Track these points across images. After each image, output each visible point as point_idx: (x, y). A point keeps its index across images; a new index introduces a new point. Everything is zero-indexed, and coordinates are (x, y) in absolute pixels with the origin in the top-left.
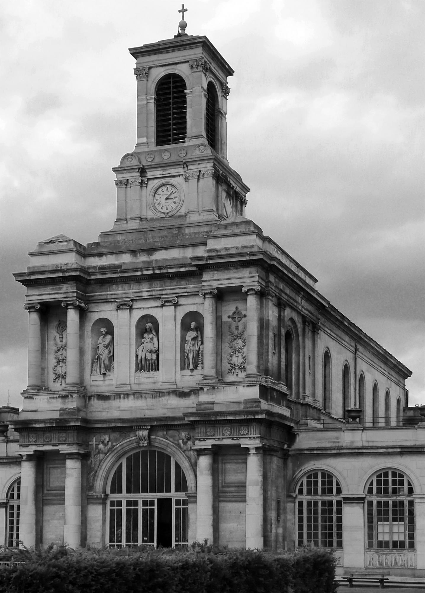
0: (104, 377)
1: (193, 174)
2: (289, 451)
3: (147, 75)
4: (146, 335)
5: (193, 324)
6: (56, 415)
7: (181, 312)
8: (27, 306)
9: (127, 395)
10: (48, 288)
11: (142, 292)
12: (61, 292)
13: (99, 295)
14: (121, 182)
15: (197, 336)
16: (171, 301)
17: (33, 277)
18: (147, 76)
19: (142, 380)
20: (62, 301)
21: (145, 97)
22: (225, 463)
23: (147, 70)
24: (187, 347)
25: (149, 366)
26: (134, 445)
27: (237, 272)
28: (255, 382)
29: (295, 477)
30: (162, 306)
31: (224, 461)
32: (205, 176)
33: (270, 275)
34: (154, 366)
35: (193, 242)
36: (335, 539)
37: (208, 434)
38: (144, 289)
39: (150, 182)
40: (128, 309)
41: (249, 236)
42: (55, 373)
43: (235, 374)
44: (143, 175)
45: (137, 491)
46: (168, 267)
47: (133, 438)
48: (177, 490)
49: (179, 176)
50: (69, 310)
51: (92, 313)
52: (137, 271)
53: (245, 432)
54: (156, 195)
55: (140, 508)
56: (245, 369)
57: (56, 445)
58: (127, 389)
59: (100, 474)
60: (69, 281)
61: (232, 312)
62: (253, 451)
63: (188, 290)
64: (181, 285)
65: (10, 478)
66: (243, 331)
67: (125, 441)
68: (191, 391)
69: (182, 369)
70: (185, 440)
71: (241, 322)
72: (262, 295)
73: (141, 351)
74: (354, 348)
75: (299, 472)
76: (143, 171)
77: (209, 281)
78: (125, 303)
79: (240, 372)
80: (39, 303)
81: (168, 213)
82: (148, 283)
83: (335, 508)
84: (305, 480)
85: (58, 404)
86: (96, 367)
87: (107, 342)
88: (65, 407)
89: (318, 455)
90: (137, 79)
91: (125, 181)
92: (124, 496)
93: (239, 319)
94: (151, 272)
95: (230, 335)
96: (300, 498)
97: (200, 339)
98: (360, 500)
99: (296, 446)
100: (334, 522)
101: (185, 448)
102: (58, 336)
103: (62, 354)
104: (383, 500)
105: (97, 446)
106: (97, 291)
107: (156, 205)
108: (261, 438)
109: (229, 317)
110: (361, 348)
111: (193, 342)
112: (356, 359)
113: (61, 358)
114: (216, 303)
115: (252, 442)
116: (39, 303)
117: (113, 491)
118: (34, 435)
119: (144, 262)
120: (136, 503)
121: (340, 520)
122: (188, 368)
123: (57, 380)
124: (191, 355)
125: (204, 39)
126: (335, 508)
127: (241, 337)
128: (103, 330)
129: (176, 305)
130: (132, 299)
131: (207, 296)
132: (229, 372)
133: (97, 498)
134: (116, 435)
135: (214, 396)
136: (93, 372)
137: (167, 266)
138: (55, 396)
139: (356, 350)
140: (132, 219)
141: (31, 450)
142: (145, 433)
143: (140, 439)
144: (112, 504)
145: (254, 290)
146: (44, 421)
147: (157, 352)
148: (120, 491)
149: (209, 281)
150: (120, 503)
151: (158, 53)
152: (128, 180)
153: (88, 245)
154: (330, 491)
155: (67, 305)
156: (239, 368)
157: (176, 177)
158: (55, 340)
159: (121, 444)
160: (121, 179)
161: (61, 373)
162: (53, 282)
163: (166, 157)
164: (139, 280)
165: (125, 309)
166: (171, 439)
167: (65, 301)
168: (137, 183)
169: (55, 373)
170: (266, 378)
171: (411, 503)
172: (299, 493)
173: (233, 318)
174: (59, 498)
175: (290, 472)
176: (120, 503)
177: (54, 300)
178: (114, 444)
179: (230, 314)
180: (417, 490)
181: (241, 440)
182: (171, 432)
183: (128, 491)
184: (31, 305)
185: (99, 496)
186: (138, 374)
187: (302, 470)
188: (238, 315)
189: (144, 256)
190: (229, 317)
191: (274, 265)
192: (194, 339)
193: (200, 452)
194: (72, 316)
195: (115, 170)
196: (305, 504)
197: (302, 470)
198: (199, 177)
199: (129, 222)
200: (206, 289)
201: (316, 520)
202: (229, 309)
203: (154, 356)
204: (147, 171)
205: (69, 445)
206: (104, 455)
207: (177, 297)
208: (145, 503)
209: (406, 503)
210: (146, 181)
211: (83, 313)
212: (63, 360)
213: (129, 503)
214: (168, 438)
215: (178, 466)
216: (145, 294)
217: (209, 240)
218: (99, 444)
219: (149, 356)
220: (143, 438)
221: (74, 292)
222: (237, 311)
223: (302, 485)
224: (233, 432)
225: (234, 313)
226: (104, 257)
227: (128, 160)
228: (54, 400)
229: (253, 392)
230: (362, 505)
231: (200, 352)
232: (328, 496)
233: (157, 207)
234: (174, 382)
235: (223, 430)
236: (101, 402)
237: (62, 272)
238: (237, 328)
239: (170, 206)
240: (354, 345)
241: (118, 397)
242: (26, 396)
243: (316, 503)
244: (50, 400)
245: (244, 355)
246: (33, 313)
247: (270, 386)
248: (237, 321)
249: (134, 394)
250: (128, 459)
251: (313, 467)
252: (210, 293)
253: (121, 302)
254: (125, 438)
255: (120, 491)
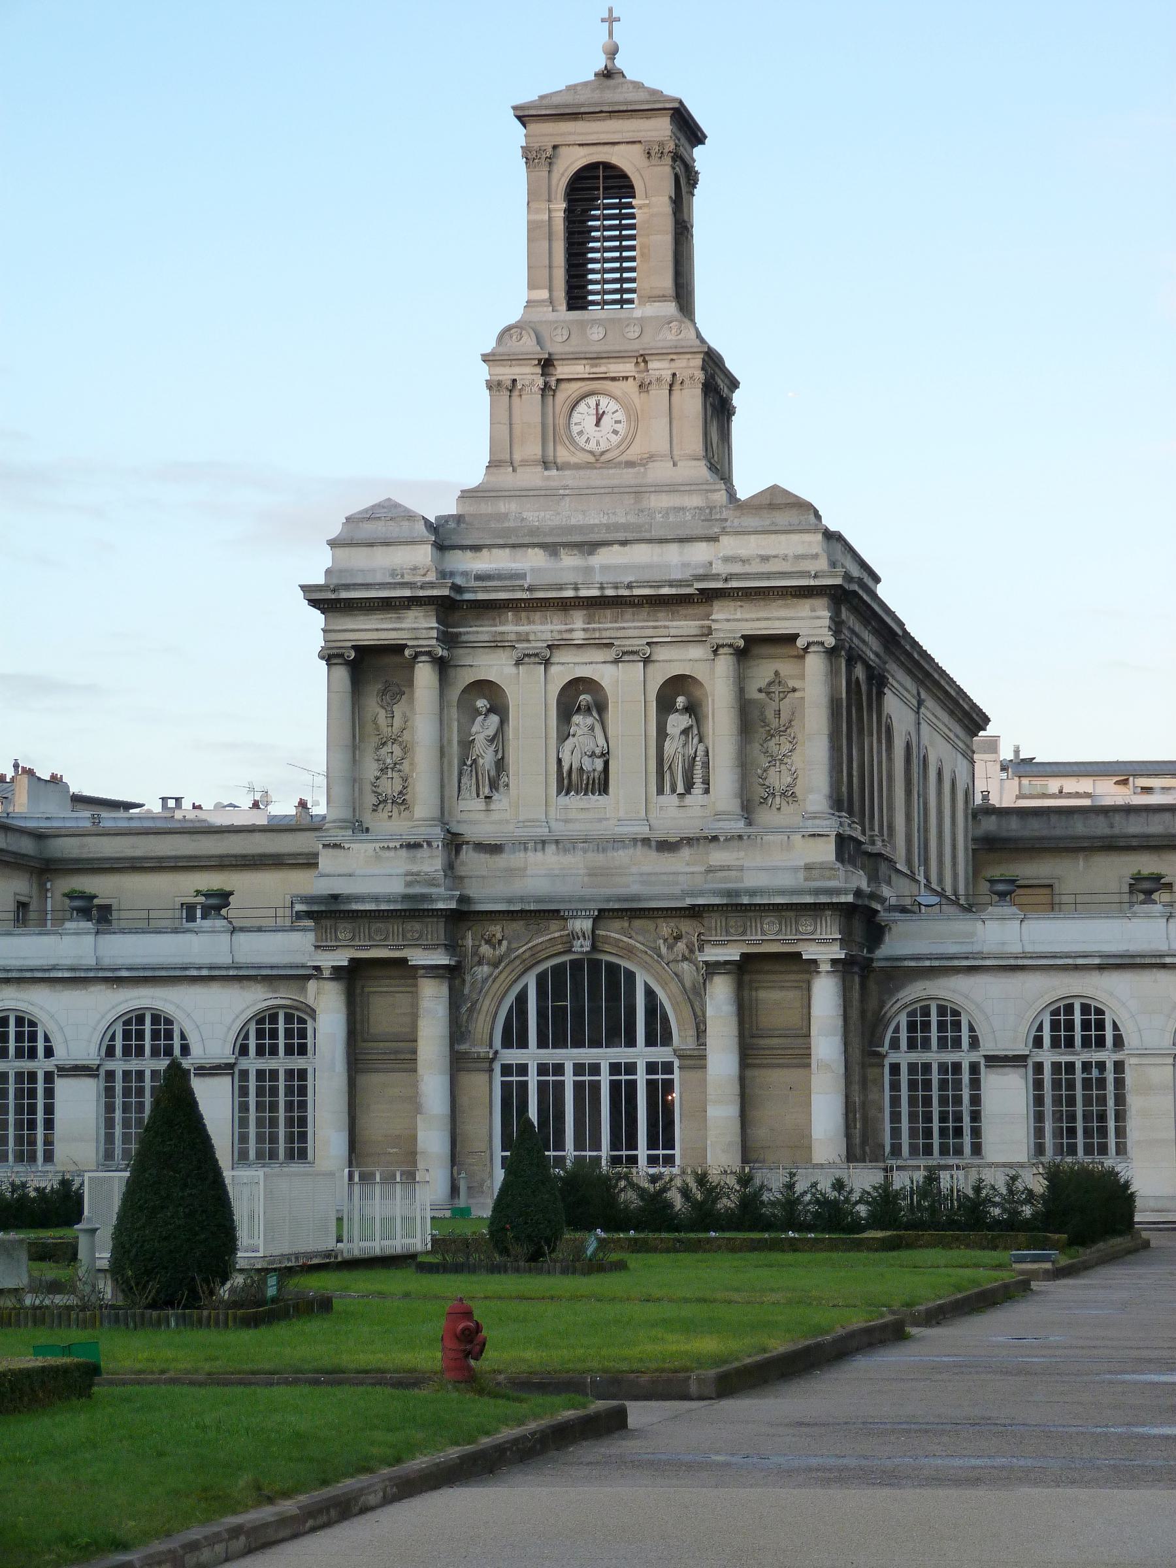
0: (487, 804)
1: (659, 380)
2: (872, 960)
3: (550, 161)
4: (577, 719)
5: (681, 701)
6: (397, 887)
7: (659, 676)
8: (326, 652)
9: (542, 843)
10: (376, 617)
11: (571, 630)
12: (403, 626)
13: (474, 633)
14: (499, 384)
15: (691, 726)
16: (633, 653)
17: (344, 595)
18: (550, 164)
19: (573, 815)
20: (405, 646)
21: (545, 205)
22: (757, 989)
23: (550, 152)
24: (670, 747)
25: (587, 784)
26: (560, 948)
27: (786, 606)
28: (829, 830)
29: (886, 1013)
30: (616, 661)
31: (755, 985)
32: (686, 385)
33: (843, 609)
34: (601, 785)
35: (682, 533)
36: (967, 1140)
37: (732, 931)
38: (577, 625)
39: (564, 386)
40: (541, 663)
41: (807, 535)
42: (375, 792)
43: (774, 808)
44: (546, 370)
45: (560, 1043)
46: (635, 584)
47: (556, 935)
48: (650, 1041)
49: (627, 378)
50: (421, 665)
51: (459, 668)
52: (567, 589)
53: (809, 928)
54: (575, 414)
55: (569, 1079)
56: (795, 797)
57: (398, 947)
58: (543, 831)
59: (485, 1008)
60: (421, 605)
61: (767, 680)
62: (825, 967)
63: (673, 632)
64: (657, 621)
65: (243, 1011)
66: (791, 721)
67: (540, 940)
68: (682, 839)
69: (660, 791)
70: (671, 941)
71: (786, 701)
72: (832, 653)
73: (570, 753)
74: (913, 696)
75: (894, 1004)
76: (547, 364)
77: (728, 620)
78: (538, 651)
79: (784, 803)
80: (354, 647)
81: (603, 453)
82: (585, 612)
83: (966, 1077)
84: (903, 1019)
85: (400, 863)
86: (469, 783)
87: (491, 732)
88: (415, 869)
89: (932, 969)
90: (528, 168)
91: (509, 383)
92: (532, 1055)
93: (781, 695)
94: (595, 593)
95: (763, 727)
96: (893, 1058)
97: (696, 732)
98: (1016, 1061)
99: (884, 950)
100: (964, 1106)
101: (671, 958)
102: (382, 714)
103: (392, 753)
104: (1063, 1061)
105: (476, 947)
106: (472, 624)
107: (574, 433)
108: (844, 943)
109: (760, 691)
110: (930, 703)
111: (683, 737)
112: (919, 724)
113: (389, 761)
114: (739, 661)
115: (822, 948)
116: (354, 647)
117: (507, 1043)
118: (349, 926)
119: (576, 569)
120: (559, 1069)
121: (976, 1100)
122: (673, 790)
123: (381, 806)
124: (680, 765)
125: (676, 105)
126: (966, 1077)
127: (785, 731)
128: (481, 703)
129: (647, 661)
130: (550, 643)
131: (721, 651)
132: (761, 803)
133: (479, 1058)
134: (518, 926)
135: (742, 854)
136: (462, 792)
137: (631, 582)
138: (392, 845)
139: (920, 703)
140: (525, 463)
141: (341, 958)
142: (587, 925)
143: (573, 936)
144: (506, 1070)
145: (822, 643)
146: (376, 898)
147: (605, 755)
148: (523, 1044)
149: (728, 620)
150: (523, 1069)
151: (575, 119)
152: (514, 381)
153: (437, 518)
154: (957, 1043)
155: (417, 655)
156: (783, 794)
157: (619, 380)
158: (375, 722)
159: (530, 945)
160: (500, 378)
161: (390, 792)
162: (387, 605)
163: (596, 337)
164: (565, 605)
165: (535, 663)
166: (640, 938)
167: (413, 646)
168: (535, 389)
169: (375, 792)
170: (839, 817)
171: (1119, 1066)
172: (890, 1048)
173: (768, 693)
174: (392, 1057)
175: (873, 1004)
176: (523, 1069)
177: (386, 642)
178: (514, 946)
179: (762, 684)
180: (1130, 1039)
181: (801, 943)
182: (637, 923)
183: (542, 1043)
184: (335, 651)
185: (482, 1055)
186: (564, 800)
187: (898, 1000)
188: (777, 687)
189: (575, 555)
190: (760, 691)
191: (855, 592)
192: (686, 732)
193: (712, 968)
194: (425, 675)
195: (486, 359)
196: (904, 1070)
197: (898, 1000)
198: (671, 386)
199: (519, 470)
200: (719, 637)
201: (927, 1101)
202: (763, 671)
203: (599, 764)
204: (555, 363)
205: (426, 947)
206: (491, 968)
207: (648, 644)
208: (579, 1069)
209: (1110, 1066)
210: (553, 384)
211: (443, 666)
212: (395, 764)
213: (543, 1069)
214: (634, 934)
215: (650, 994)
216: (579, 636)
217: (724, 537)
218: (479, 946)
219: (587, 764)
220: (580, 934)
221: (432, 628)
222: (777, 678)
223: (897, 1030)
224: (784, 928)
225: (770, 684)
226: (485, 551)
227: (511, 337)
228: (392, 854)
229: (826, 851)
230: (1024, 1070)
231: (698, 759)
232: (952, 1052)
233: (577, 439)
234: (644, 820)
235: (762, 924)
236: (484, 857)
237: (411, 588)
238: (778, 713)
239: (605, 438)
240: (915, 692)
241: (522, 847)
242: (328, 843)
243: (927, 1067)
244: (382, 853)
245: (793, 769)
246: (338, 667)
247: (848, 833)
248: (777, 700)
249: (557, 842)
250: (541, 979)
251: (923, 994)
252: (731, 646)
253: (528, 648)
254: (539, 933)
255: (523, 1044)
